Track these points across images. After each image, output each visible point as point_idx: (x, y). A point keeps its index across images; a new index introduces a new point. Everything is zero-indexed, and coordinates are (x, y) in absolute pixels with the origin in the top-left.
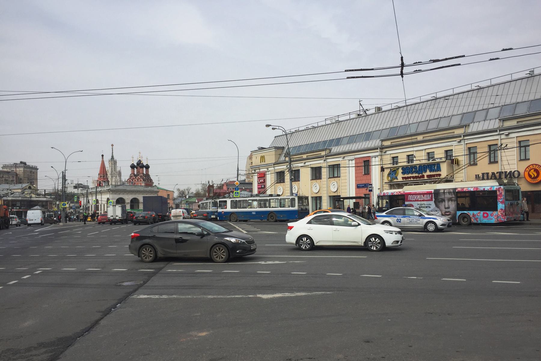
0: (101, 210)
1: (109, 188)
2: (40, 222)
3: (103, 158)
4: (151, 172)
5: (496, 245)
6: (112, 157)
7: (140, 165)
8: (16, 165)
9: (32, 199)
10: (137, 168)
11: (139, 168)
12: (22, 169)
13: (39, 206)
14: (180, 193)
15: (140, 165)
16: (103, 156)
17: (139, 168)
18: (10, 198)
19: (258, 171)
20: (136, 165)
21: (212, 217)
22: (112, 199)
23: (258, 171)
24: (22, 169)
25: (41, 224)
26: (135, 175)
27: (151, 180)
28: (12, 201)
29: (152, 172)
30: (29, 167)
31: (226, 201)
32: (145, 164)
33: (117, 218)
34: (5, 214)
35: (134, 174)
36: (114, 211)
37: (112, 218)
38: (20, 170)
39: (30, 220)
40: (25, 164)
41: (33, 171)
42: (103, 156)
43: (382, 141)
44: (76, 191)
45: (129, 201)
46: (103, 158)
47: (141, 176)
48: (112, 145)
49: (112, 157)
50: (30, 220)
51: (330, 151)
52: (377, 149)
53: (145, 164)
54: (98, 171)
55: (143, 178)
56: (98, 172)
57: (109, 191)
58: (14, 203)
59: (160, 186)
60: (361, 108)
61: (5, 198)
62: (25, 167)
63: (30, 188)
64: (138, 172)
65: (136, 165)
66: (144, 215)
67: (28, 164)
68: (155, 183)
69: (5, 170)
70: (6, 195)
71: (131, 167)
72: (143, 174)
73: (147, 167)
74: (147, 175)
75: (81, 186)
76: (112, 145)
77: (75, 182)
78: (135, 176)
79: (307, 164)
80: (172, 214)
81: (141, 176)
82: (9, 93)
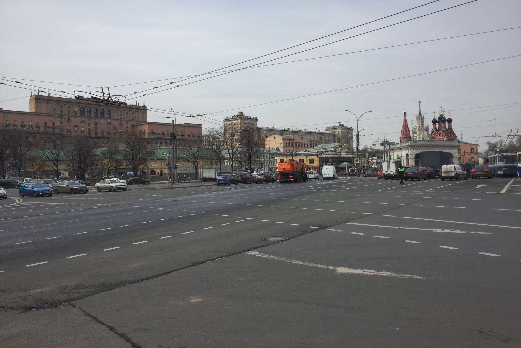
1: (407, 144)
2: (332, 176)
3: (405, 116)
4: (454, 125)
5: (444, 224)
6: (420, 114)
7: (442, 119)
8: (335, 128)
9: (342, 156)
10: (439, 123)
11: (440, 122)
12: (340, 130)
13: (347, 162)
14: (491, 146)
15: (442, 119)
16: (405, 113)
17: (440, 122)
18: (324, 156)
20: (437, 119)
21: (499, 172)
22: (411, 154)
24: (340, 130)
25: (334, 178)
26: (436, 130)
27: (454, 134)
28: (326, 158)
29: (455, 127)
30: (346, 128)
32: (447, 118)
33: (392, 173)
34: (302, 169)
35: (436, 129)
36: (389, 167)
37: (386, 173)
38: (339, 132)
39: (325, 175)
40: (343, 126)
41: (349, 131)
42: (405, 113)
44: (382, 148)
45: (414, 156)
46: (405, 116)
47: (443, 131)
48: (420, 102)
49: (420, 114)
50: (325, 175)
53: (447, 118)
54: (400, 127)
55: (445, 133)
57: (408, 147)
58: (327, 160)
59: (464, 140)
61: (320, 156)
62: (281, 134)
63: (341, 146)
64: (440, 127)
65: (437, 119)
66: (414, 170)
67: (345, 125)
68: (459, 138)
69: (328, 132)
70: (322, 153)
71: (432, 122)
72: (445, 128)
73: (450, 121)
75: (388, 143)
76: (420, 102)
77: (382, 140)
80: (443, 170)
81: (443, 131)
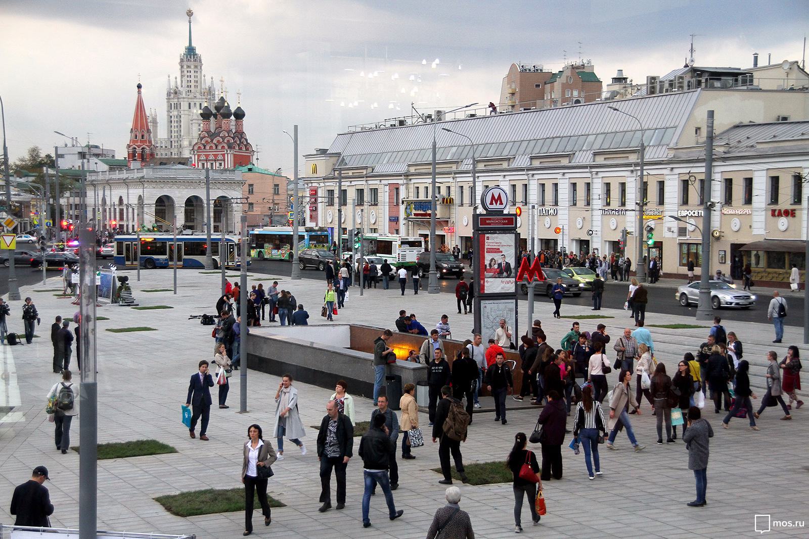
0: (128, 220)
3: (139, 92)
16: (139, 87)
19: (310, 185)
20: (214, 111)
23: (310, 185)
31: (118, 254)
43: (409, 166)
46: (139, 92)
47: (223, 138)
51: (373, 170)
52: (401, 176)
56: (130, 125)
60: (414, 113)
72: (229, 131)
73: (239, 115)
74: (240, 134)
78: (212, 136)
79: (353, 183)
82: (132, 536)
